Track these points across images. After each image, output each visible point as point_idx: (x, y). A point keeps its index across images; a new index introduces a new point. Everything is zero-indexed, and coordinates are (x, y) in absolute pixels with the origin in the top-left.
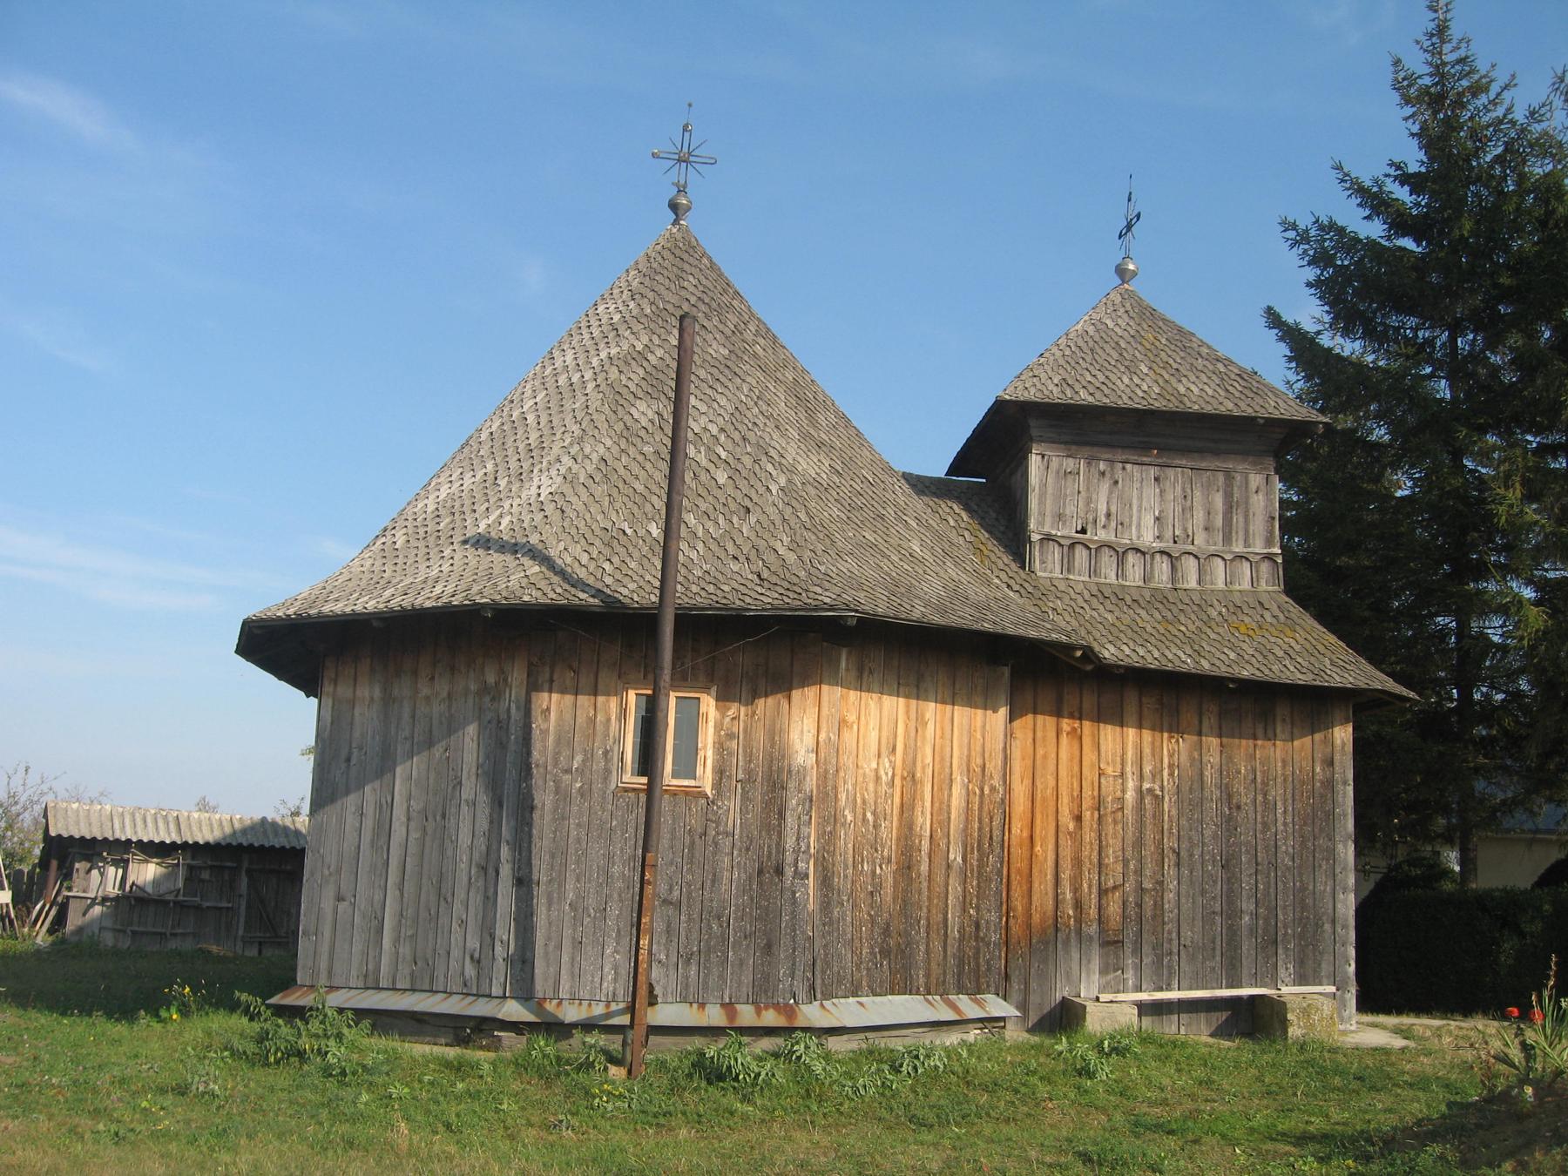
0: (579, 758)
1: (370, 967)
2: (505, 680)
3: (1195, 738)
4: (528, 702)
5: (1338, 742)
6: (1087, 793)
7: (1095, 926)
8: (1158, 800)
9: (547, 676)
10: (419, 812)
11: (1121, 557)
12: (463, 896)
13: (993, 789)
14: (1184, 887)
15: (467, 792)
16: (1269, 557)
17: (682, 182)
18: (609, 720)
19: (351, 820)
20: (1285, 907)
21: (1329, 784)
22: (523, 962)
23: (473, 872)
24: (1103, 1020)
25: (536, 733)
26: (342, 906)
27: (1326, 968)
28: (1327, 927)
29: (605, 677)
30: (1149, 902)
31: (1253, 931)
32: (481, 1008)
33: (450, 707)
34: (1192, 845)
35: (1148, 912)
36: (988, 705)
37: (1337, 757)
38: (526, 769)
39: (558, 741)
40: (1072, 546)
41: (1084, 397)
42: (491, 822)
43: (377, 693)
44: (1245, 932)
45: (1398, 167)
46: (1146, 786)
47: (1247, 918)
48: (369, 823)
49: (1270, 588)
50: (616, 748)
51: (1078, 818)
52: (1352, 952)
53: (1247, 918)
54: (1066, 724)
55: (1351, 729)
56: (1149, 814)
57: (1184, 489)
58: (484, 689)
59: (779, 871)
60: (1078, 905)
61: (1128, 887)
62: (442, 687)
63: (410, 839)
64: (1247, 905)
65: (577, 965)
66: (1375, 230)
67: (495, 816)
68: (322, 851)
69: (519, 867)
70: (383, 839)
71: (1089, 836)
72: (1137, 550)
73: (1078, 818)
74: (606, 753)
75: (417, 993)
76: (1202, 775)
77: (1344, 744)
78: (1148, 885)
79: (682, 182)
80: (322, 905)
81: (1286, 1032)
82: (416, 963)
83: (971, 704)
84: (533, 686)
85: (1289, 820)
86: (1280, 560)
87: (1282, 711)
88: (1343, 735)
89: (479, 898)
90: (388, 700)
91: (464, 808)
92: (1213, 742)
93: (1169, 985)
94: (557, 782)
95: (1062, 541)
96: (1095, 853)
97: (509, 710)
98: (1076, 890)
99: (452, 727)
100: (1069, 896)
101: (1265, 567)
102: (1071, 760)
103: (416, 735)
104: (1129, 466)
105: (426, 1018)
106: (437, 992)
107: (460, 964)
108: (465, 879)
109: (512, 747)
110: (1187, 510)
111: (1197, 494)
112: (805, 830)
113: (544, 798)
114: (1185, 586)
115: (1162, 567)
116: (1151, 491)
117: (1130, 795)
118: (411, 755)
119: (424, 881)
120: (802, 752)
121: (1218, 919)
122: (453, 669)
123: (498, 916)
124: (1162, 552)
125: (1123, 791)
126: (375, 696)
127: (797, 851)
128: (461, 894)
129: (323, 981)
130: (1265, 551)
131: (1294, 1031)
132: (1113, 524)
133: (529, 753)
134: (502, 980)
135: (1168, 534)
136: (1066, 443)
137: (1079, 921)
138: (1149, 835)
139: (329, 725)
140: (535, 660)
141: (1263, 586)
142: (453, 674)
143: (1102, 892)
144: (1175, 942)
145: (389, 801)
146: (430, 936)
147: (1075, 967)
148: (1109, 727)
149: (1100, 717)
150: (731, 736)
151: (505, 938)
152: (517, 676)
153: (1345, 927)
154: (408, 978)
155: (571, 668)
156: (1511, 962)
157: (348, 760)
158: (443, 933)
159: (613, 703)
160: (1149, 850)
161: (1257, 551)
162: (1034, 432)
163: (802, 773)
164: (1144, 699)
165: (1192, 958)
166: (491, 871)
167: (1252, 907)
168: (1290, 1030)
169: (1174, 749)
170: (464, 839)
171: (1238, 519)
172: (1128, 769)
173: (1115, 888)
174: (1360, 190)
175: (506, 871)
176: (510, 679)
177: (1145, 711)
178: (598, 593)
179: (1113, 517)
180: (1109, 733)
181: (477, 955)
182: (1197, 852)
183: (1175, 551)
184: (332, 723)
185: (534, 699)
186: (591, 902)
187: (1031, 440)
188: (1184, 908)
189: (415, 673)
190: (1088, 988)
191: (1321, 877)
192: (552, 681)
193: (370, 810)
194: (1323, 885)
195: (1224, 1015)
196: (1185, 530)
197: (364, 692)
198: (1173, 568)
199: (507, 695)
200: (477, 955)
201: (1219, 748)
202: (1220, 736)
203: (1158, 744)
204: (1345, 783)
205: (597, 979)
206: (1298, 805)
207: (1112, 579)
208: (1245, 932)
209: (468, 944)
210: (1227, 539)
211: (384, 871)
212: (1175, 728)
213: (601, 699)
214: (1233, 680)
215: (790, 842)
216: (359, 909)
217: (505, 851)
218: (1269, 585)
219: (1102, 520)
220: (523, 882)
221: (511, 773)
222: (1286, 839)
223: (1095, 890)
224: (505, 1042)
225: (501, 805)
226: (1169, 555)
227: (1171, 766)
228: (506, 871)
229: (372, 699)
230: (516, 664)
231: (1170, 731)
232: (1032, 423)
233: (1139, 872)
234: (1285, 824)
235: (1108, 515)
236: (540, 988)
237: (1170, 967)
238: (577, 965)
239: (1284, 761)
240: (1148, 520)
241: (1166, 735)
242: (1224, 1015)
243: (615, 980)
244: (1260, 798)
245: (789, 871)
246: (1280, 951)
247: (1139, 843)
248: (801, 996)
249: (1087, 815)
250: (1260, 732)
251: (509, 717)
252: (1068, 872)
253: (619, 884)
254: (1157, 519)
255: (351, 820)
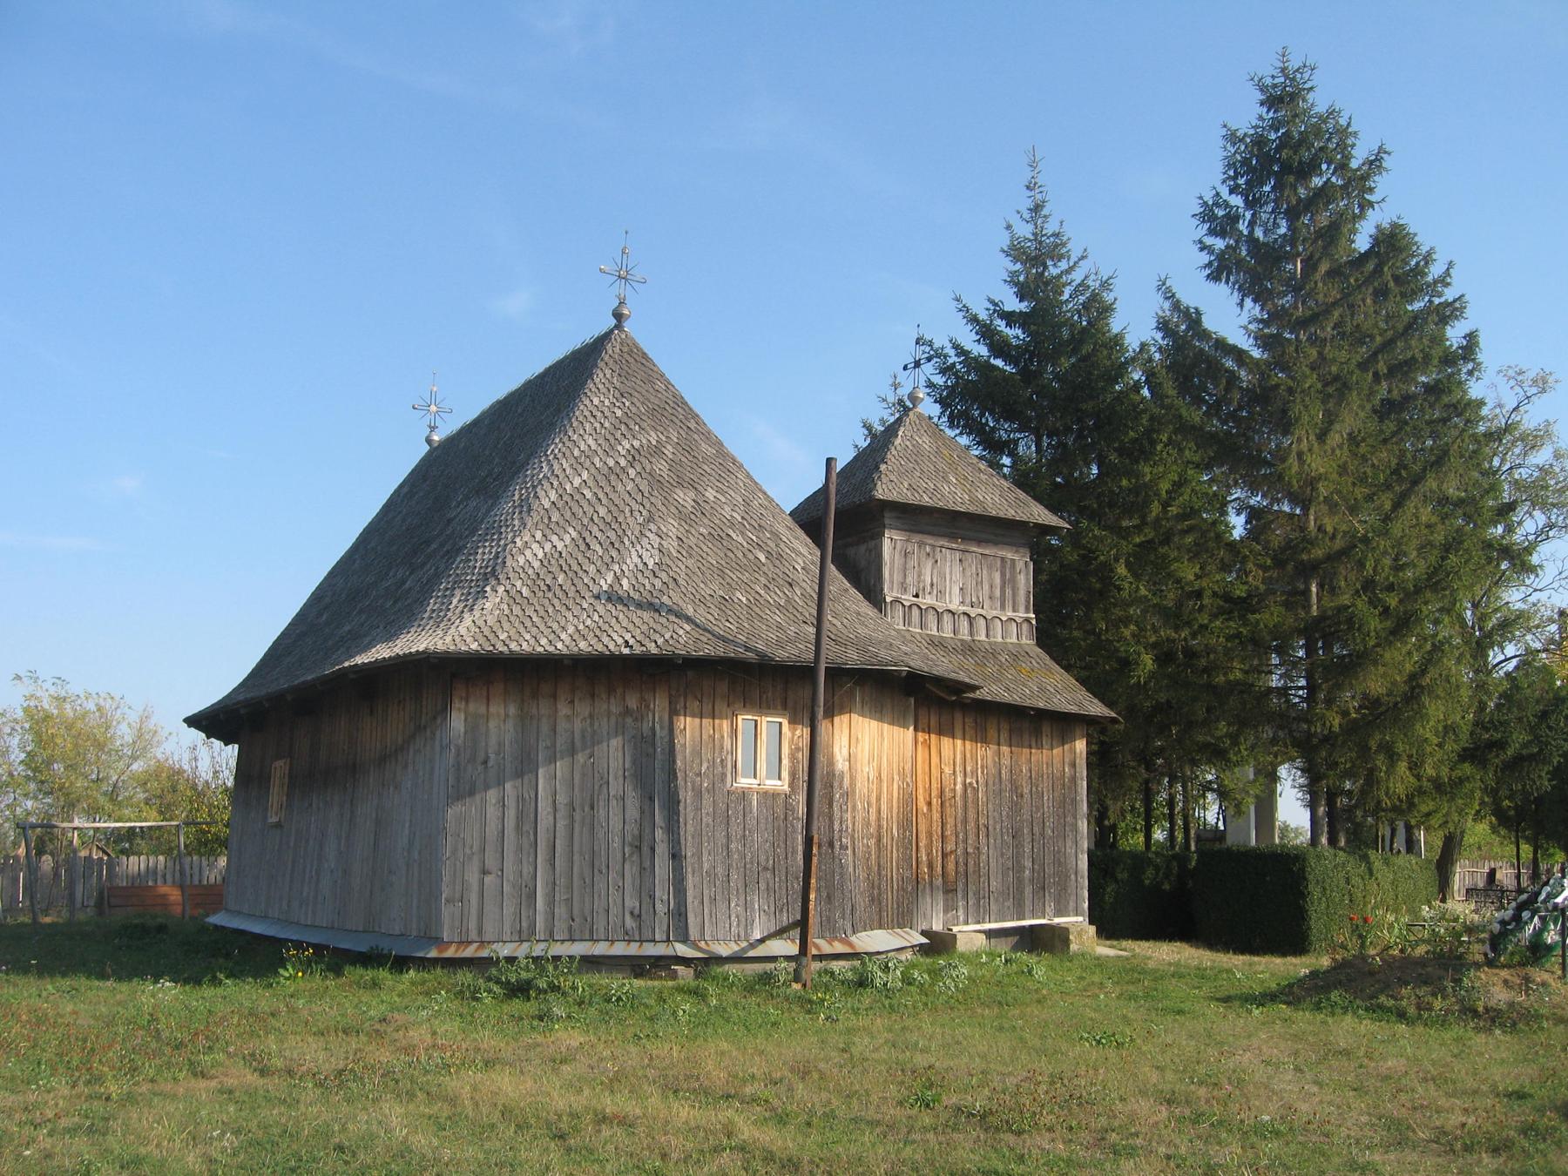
0: (705, 766)
1: (524, 924)
2: (647, 707)
3: (996, 747)
4: (671, 723)
5: (1078, 751)
6: (934, 785)
7: (940, 879)
8: (976, 790)
9: (682, 705)
10: (566, 805)
11: (939, 615)
12: (618, 867)
13: (907, 784)
14: (991, 852)
15: (615, 787)
16: (1027, 620)
17: (622, 296)
18: (723, 737)
19: (492, 812)
20: (1049, 864)
21: (1074, 779)
22: (679, 915)
23: (626, 850)
24: (966, 943)
25: (678, 747)
26: (488, 879)
27: (1072, 904)
28: (1073, 877)
29: (721, 706)
30: (971, 863)
31: (1032, 880)
32: (651, 950)
33: (592, 725)
34: (995, 822)
35: (971, 870)
36: (906, 727)
37: (1078, 761)
38: (672, 774)
39: (692, 753)
40: (910, 606)
41: (926, 500)
42: (642, 812)
43: (512, 710)
44: (1027, 881)
45: (996, 304)
46: (968, 781)
47: (1027, 872)
48: (511, 814)
49: (1028, 642)
50: (729, 757)
51: (929, 804)
52: (1086, 894)
53: (1027, 872)
54: (921, 736)
55: (1085, 743)
56: (970, 800)
57: (977, 568)
58: (627, 712)
59: (831, 845)
60: (931, 866)
61: (959, 851)
62: (583, 709)
63: (558, 825)
64: (1028, 864)
65: (714, 916)
66: (981, 350)
67: (646, 808)
68: (462, 836)
69: (673, 847)
70: (527, 827)
71: (936, 816)
72: (950, 611)
73: (929, 804)
74: (722, 761)
75: (576, 943)
76: (1000, 773)
77: (1081, 753)
78: (970, 850)
79: (622, 296)
80: (466, 878)
81: (1069, 948)
82: (573, 920)
83: (892, 723)
84: (674, 712)
85: (1051, 805)
86: (1034, 622)
87: (1046, 728)
88: (1081, 746)
89: (635, 869)
90: (523, 719)
91: (613, 802)
92: (1005, 749)
93: (984, 919)
94: (693, 783)
95: (905, 603)
96: (940, 828)
97: (653, 729)
98: (929, 854)
99: (592, 740)
100: (924, 858)
101: (1025, 626)
102: (924, 762)
103: (558, 745)
104: (943, 550)
105: (601, 960)
106: (598, 941)
107: (620, 917)
108: (619, 856)
109: (659, 756)
110: (980, 583)
111: (985, 572)
112: (845, 816)
113: (686, 795)
114: (978, 638)
115: (964, 624)
116: (957, 568)
117: (959, 787)
118: (552, 760)
119: (575, 858)
120: (841, 761)
121: (1011, 873)
122: (593, 696)
123: (657, 882)
124: (964, 613)
125: (955, 784)
126: (511, 714)
127: (841, 831)
128: (615, 866)
129: (473, 935)
130: (1026, 615)
131: (1074, 947)
132: (935, 592)
133: (674, 762)
134: (665, 928)
135: (968, 601)
136: (905, 530)
137: (931, 876)
138: (971, 815)
139: (462, 735)
140: (673, 693)
141: (1024, 641)
142: (594, 701)
143: (944, 855)
144: (987, 889)
145: (533, 796)
146: (587, 899)
147: (929, 908)
148: (946, 739)
149: (940, 733)
150: (798, 749)
151: (665, 897)
152: (660, 704)
153: (1082, 877)
154: (566, 931)
155: (696, 697)
156: (1111, 900)
157: (485, 763)
158: (600, 896)
159: (726, 724)
160: (971, 825)
161: (1021, 615)
162: (887, 521)
163: (842, 774)
164: (966, 720)
165: (997, 900)
166: (645, 849)
167: (1030, 864)
168: (1071, 946)
169: (984, 754)
170: (615, 823)
171: (1008, 591)
172: (957, 769)
173: (951, 852)
174: (974, 319)
175: (662, 849)
176: (652, 706)
177: (967, 727)
178: (757, 653)
179: (935, 587)
180: (946, 742)
181: (636, 912)
182: (998, 827)
183: (973, 612)
184: (466, 733)
185: (675, 721)
186: (720, 870)
187: (884, 527)
188: (991, 865)
189: (554, 697)
190: (937, 923)
191: (1069, 843)
192: (685, 708)
193: (511, 803)
194: (1070, 850)
195: (1016, 938)
196: (978, 598)
197: (496, 708)
198: (971, 624)
199: (651, 719)
200: (636, 912)
201: (1009, 755)
202: (1011, 746)
203: (974, 751)
204: (1082, 779)
205: (727, 925)
206: (1056, 794)
207: (934, 632)
208: (1027, 881)
209: (626, 904)
210: (1003, 607)
211: (532, 851)
212: (985, 741)
213: (717, 721)
214: (1032, 708)
215: (836, 827)
216: (508, 881)
217: (659, 834)
218: (1028, 641)
219: (928, 588)
220: (676, 856)
221: (659, 776)
222: (1049, 817)
223: (940, 854)
224: (680, 973)
225: (652, 799)
226: (969, 616)
227: (982, 767)
228: (662, 849)
229: (507, 715)
230: (657, 695)
231: (982, 742)
232: (887, 514)
233: (965, 841)
234: (1049, 807)
235: (932, 585)
236: (693, 933)
237: (985, 907)
238: (714, 916)
239: (1047, 764)
240: (956, 590)
241: (979, 745)
242: (1016, 938)
243: (738, 925)
244: (1034, 789)
245: (837, 845)
246: (1047, 894)
247: (965, 821)
248: (849, 932)
249: (934, 801)
250: (1034, 744)
251: (654, 734)
252: (924, 842)
253: (736, 856)
254: (961, 589)
255: (492, 812)
